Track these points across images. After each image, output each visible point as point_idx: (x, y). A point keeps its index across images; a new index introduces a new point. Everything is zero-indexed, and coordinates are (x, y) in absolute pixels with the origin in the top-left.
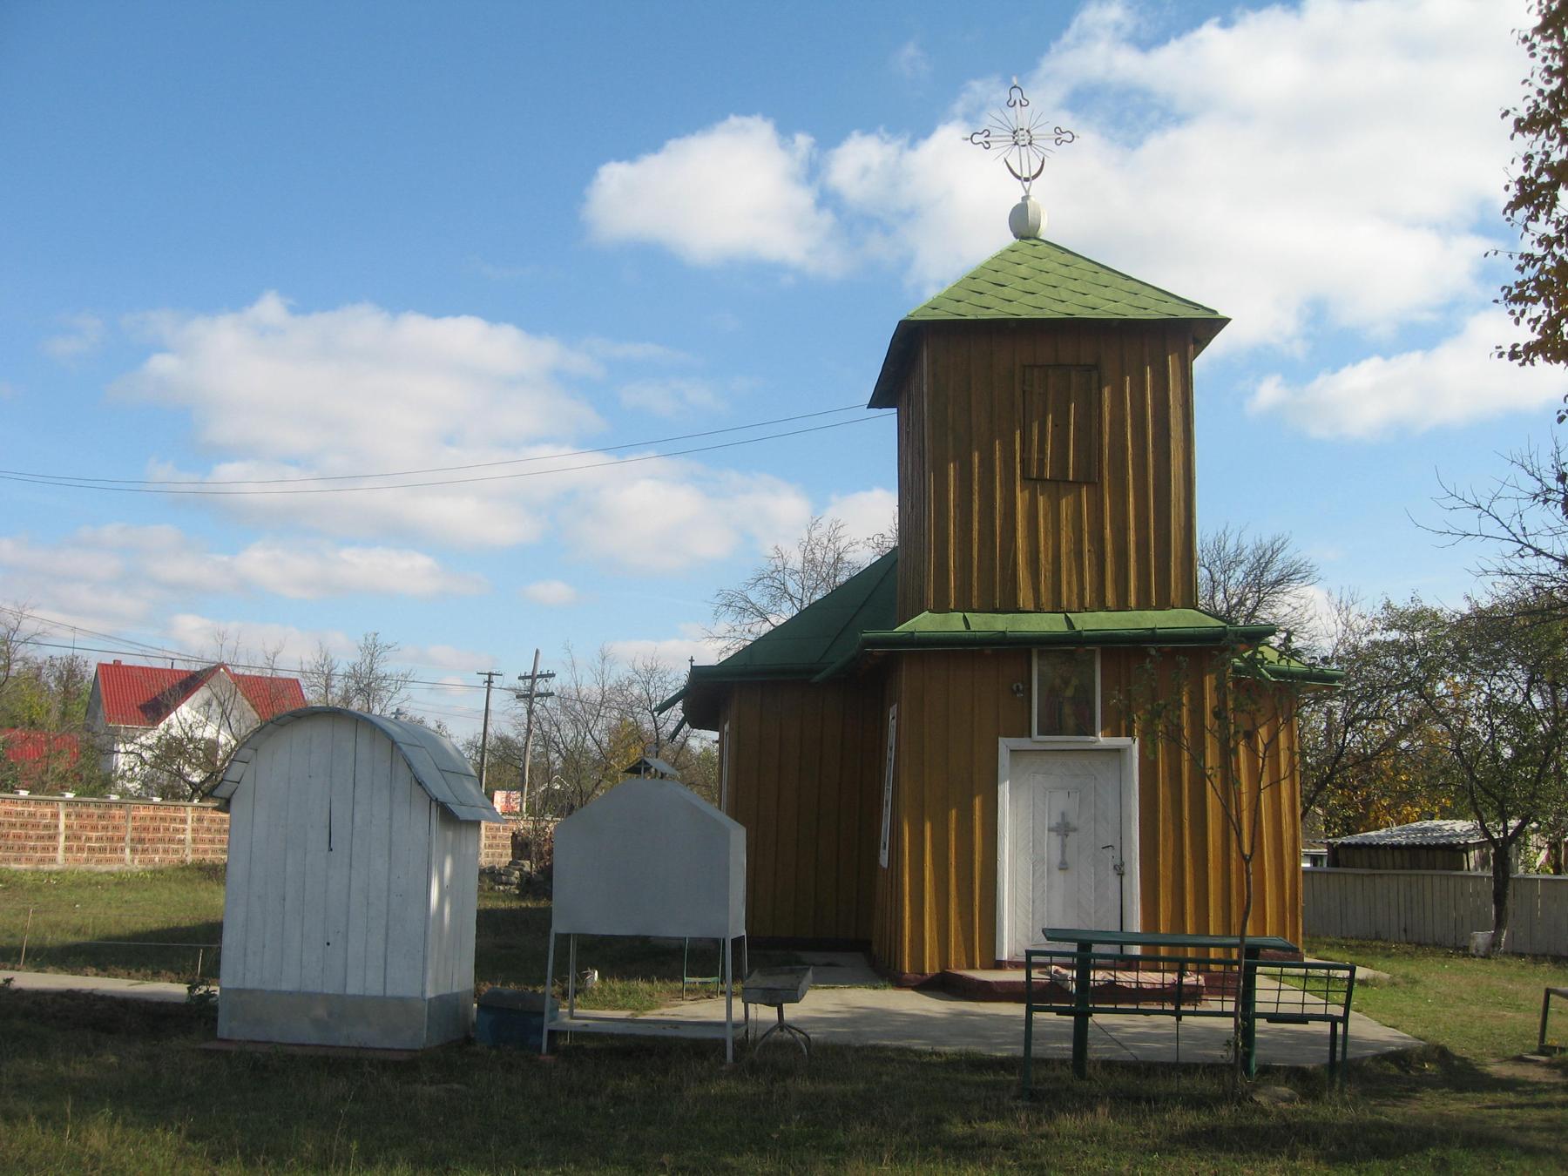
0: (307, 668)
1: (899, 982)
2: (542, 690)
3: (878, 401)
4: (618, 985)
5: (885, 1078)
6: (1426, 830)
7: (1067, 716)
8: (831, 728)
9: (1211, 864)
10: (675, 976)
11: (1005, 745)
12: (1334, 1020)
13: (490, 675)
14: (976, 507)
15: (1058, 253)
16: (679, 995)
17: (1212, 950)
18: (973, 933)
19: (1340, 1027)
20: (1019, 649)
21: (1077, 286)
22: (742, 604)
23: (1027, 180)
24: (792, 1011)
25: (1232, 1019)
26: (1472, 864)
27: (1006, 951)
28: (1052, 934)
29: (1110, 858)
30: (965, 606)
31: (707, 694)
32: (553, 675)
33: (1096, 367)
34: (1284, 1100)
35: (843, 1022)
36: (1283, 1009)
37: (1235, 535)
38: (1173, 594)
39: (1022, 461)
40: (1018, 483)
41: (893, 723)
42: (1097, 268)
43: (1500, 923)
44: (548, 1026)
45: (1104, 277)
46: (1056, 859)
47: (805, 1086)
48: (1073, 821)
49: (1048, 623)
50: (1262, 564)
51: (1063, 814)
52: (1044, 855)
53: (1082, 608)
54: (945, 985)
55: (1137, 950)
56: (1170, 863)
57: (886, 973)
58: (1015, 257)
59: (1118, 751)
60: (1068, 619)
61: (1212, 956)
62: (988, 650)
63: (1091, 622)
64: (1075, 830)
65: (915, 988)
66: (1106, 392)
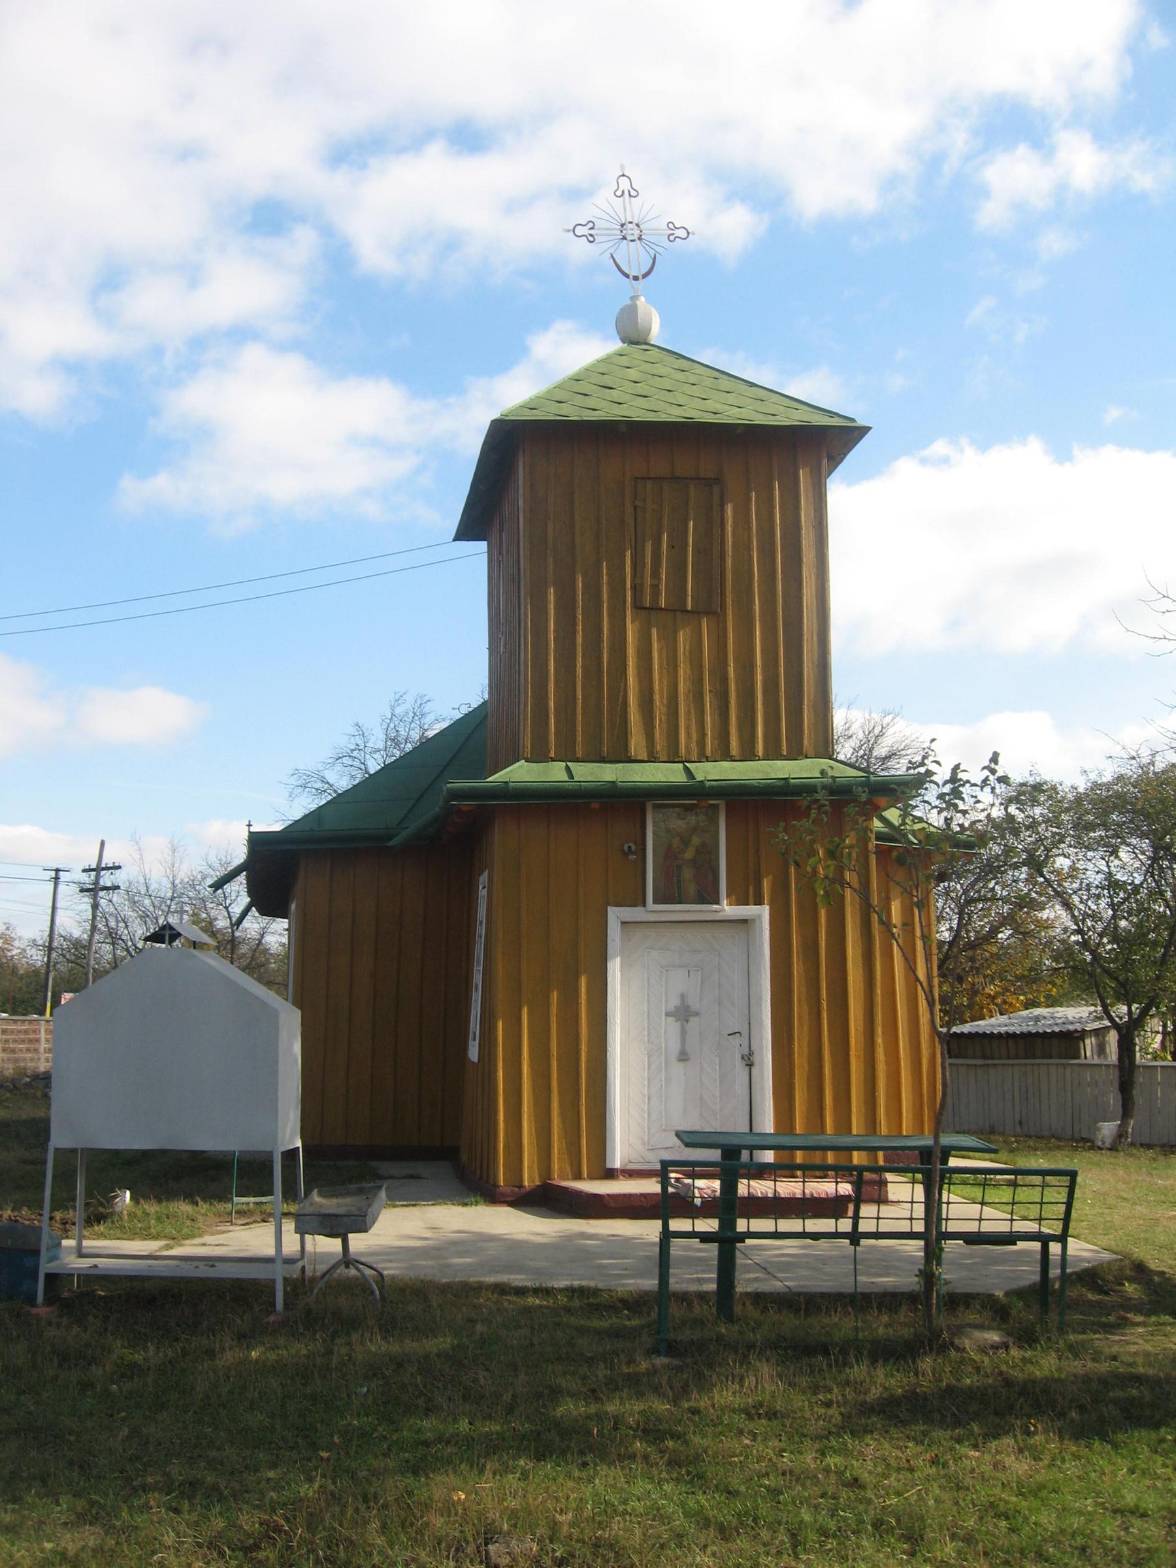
1: (492, 1197)
2: (109, 884)
3: (468, 530)
4: (152, 1208)
5: (479, 1328)
6: (1037, 1019)
7: (689, 882)
8: (412, 916)
9: (853, 1052)
10: (224, 1197)
11: (615, 915)
12: (1045, 1240)
13: (57, 870)
14: (579, 640)
15: (670, 359)
16: (228, 1218)
17: (855, 1154)
18: (579, 1137)
19: (1055, 1248)
20: (629, 803)
21: (695, 391)
22: (319, 785)
23: (636, 278)
24: (358, 1242)
25: (922, 1243)
26: (1088, 1054)
27: (617, 1160)
28: (689, 1139)
29: (736, 1047)
30: (568, 755)
31: (274, 868)
32: (119, 867)
33: (718, 480)
34: (995, 1347)
35: (423, 1252)
36: (986, 1227)
38: (806, 742)
39: (634, 587)
40: (629, 613)
41: (483, 893)
42: (717, 374)
43: (1127, 1110)
44: (46, 1267)
45: (725, 384)
46: (675, 1047)
47: (376, 1346)
48: (694, 1003)
49: (668, 774)
51: (683, 996)
52: (665, 1042)
53: (703, 758)
54: (548, 1200)
55: (769, 1157)
56: (806, 1050)
57: (477, 1185)
58: (624, 361)
60: (687, 770)
61: (856, 1161)
62: (595, 805)
63: (711, 772)
64: (697, 1014)
65: (511, 1204)
66: (729, 510)
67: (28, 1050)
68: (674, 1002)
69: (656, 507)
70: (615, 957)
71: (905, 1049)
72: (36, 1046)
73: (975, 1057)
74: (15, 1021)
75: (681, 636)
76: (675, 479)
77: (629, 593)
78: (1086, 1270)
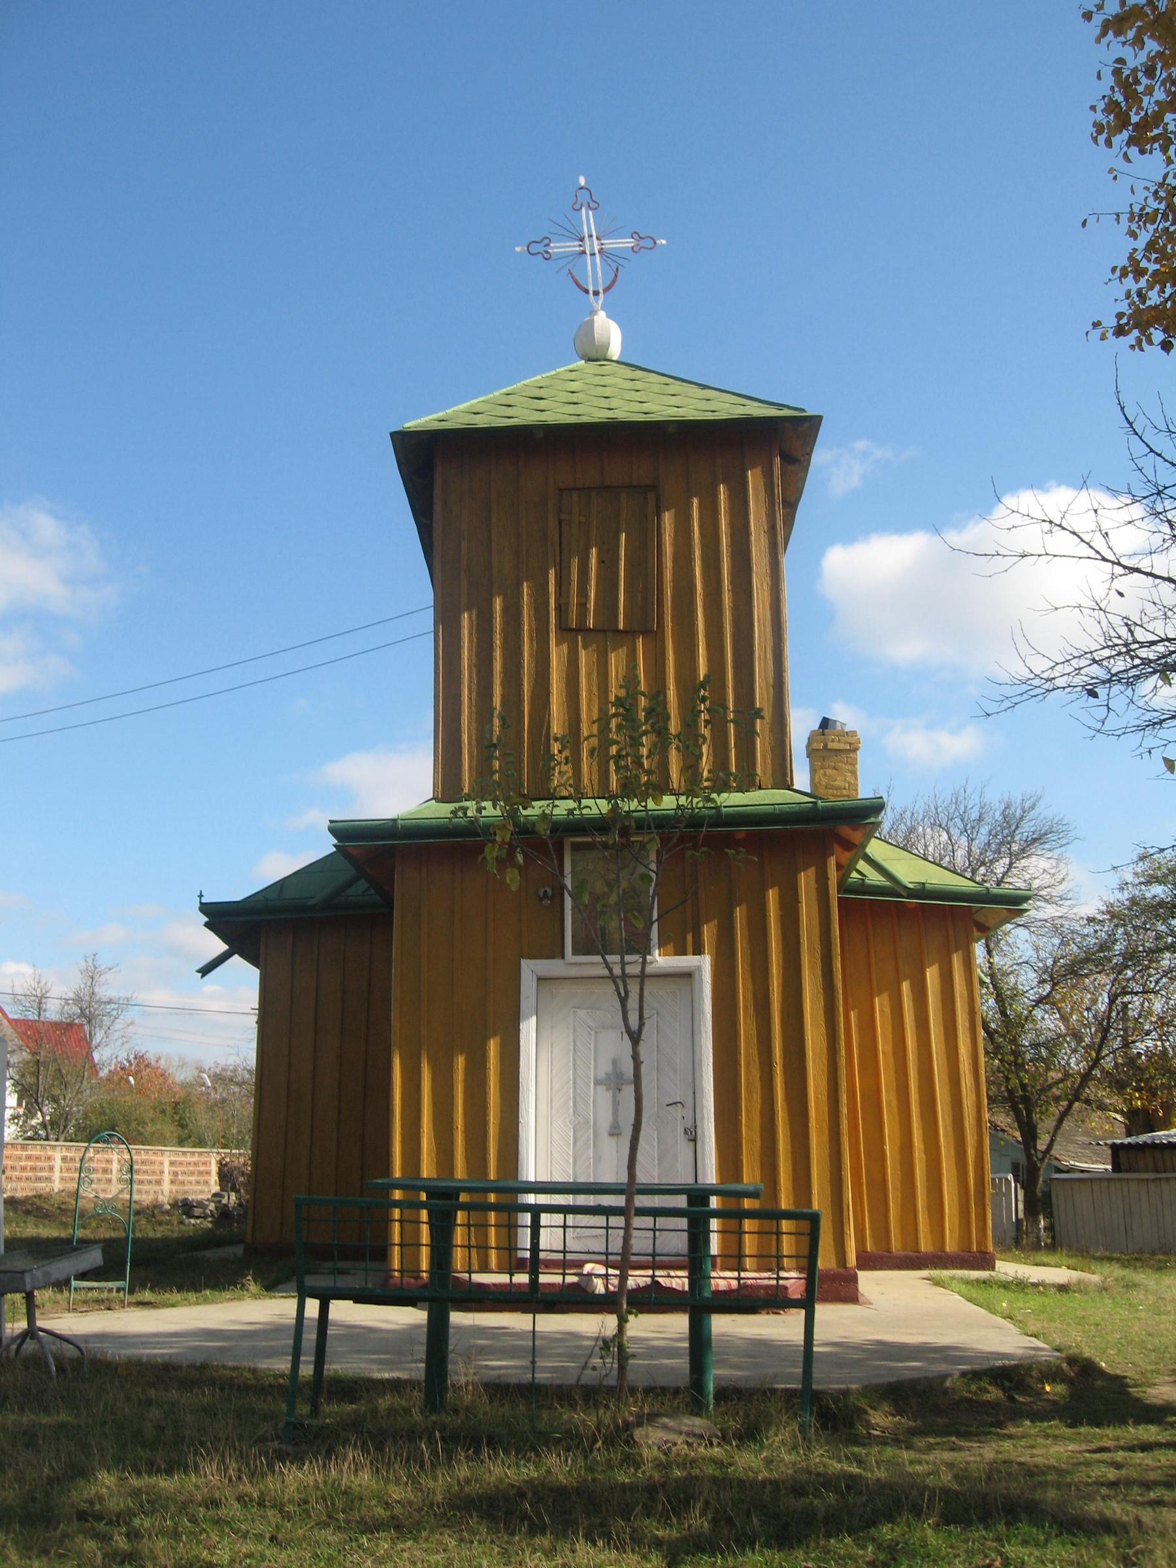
0: (18, 990)
7: (612, 935)
11: (529, 969)
33: (654, 487)
37: (976, 797)
38: (759, 771)
39: (559, 608)
40: (552, 635)
50: (1009, 824)
51: (615, 1062)
59: (688, 976)
67: (198, 1182)
68: (605, 1068)
69: (583, 519)
70: (528, 1017)
71: (946, 1136)
72: (206, 1178)
73: (1147, 1171)
74: (184, 1153)
75: (613, 657)
76: (606, 488)
77: (553, 614)
78: (1003, 1369)
